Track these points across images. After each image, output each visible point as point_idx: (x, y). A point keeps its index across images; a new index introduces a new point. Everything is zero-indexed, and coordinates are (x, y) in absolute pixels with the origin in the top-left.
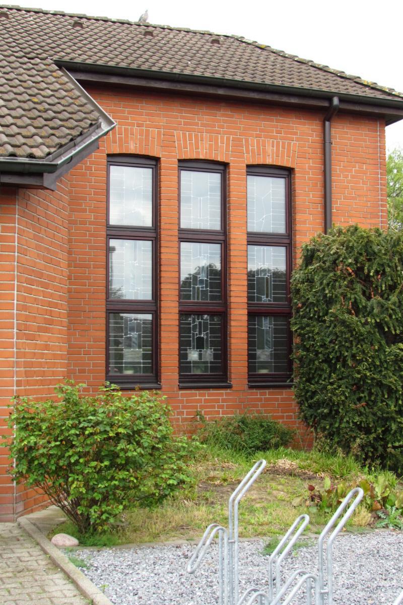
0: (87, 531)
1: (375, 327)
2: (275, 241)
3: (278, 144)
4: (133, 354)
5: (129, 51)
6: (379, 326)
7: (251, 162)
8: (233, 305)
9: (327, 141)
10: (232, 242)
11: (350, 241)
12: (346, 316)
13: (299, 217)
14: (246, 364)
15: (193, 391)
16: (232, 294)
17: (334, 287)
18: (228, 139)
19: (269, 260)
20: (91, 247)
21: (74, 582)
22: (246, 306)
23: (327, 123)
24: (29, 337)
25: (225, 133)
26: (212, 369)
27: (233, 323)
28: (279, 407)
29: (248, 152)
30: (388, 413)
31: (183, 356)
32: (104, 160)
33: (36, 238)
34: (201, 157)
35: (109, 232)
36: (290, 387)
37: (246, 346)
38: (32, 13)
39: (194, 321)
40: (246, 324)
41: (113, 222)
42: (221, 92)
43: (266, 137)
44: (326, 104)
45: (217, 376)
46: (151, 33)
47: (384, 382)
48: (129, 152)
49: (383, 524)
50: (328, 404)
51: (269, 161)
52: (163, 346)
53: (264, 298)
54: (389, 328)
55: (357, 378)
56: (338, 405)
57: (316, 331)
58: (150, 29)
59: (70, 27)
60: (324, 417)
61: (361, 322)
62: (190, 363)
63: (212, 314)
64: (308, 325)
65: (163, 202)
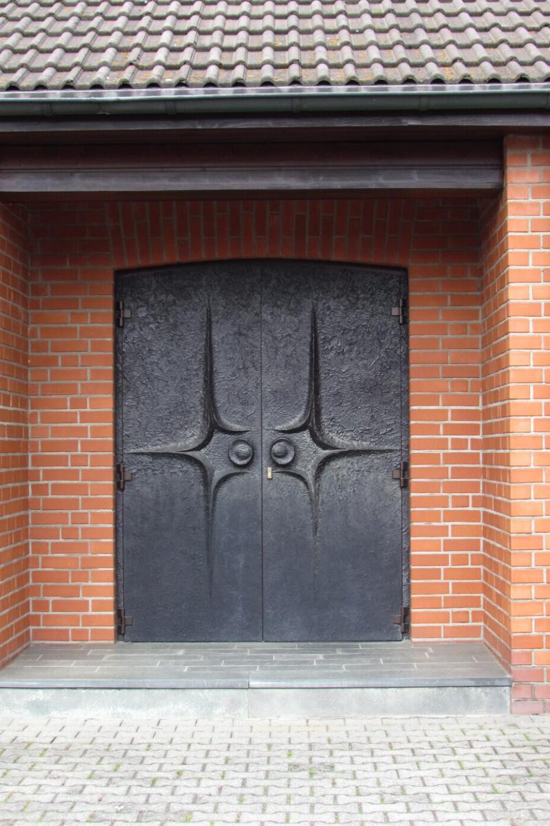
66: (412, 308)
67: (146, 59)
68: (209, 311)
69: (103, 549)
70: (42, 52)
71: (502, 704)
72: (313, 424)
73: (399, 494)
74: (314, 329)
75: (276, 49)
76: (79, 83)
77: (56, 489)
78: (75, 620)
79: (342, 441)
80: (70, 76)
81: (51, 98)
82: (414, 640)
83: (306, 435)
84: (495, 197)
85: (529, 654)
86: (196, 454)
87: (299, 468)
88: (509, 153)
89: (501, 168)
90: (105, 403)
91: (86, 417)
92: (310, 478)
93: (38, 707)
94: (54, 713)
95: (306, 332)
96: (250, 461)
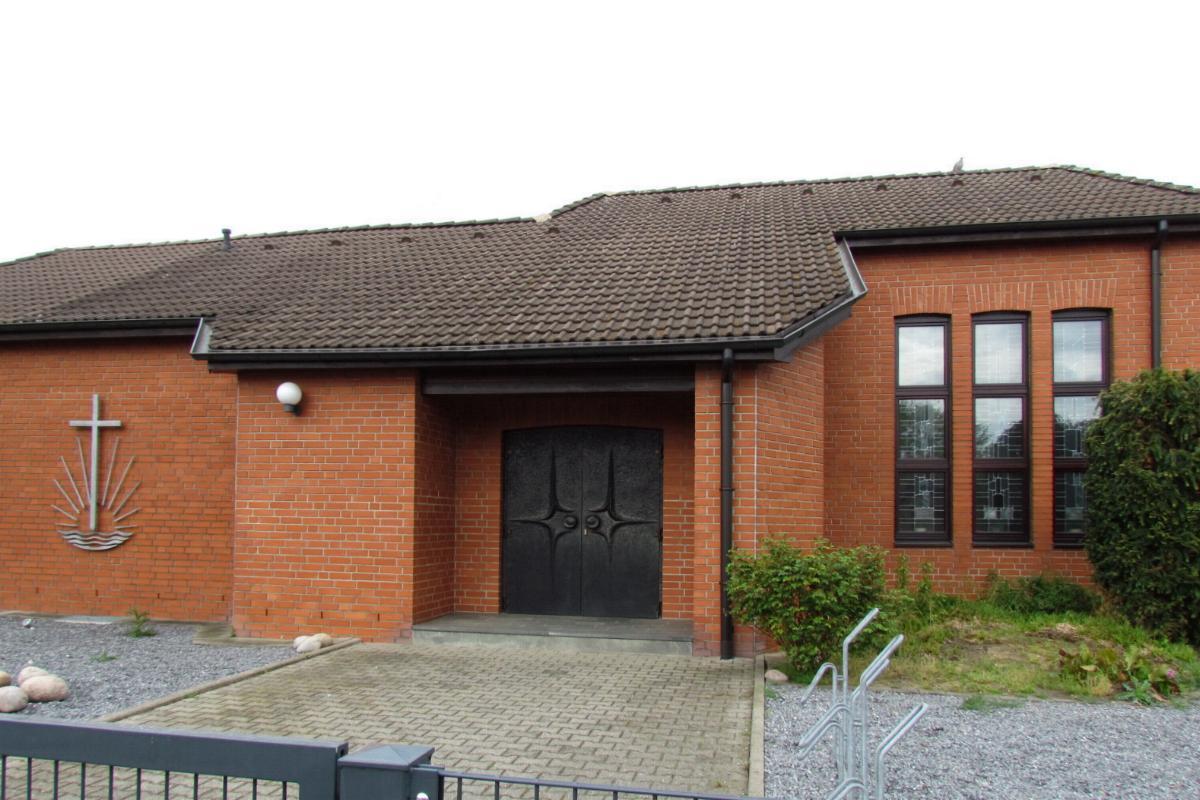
0: (798, 674)
1: (1174, 483)
2: (1087, 390)
3: (1090, 284)
4: (924, 513)
5: (1071, 194)
6: (1179, 481)
7: (1056, 308)
8: (1035, 462)
9: (1155, 272)
10: (1034, 394)
11: (1148, 387)
12: (1140, 471)
13: (1117, 362)
14: (1051, 523)
15: (988, 550)
16: (1035, 449)
17: (1126, 439)
18: (1029, 285)
19: (1079, 412)
20: (878, 410)
21: (179, 699)
22: (1051, 462)
23: (1155, 252)
24: (770, 496)
25: (1025, 279)
26: (1012, 528)
27: (1035, 480)
28: (1076, 569)
29: (1052, 297)
30: (1190, 579)
31: (977, 515)
32: (892, 323)
33: (781, 406)
34: (997, 308)
35: (898, 394)
36: (1081, 547)
37: (1051, 504)
38: (920, 179)
39: (991, 479)
40: (1051, 480)
41: (903, 382)
42: (1017, 236)
43: (1074, 278)
44: (1151, 230)
45: (1019, 534)
46: (1038, 177)
47: (1186, 544)
48: (917, 312)
49: (1126, 697)
50: (1118, 567)
51: (1079, 304)
52: (955, 504)
53: (1075, 452)
54: (1191, 483)
55: (1150, 539)
56: (1129, 568)
57: (1105, 487)
58: (1037, 174)
59: (1027, 182)
60: (1116, 580)
61: (1156, 477)
62: (986, 521)
63: (938, 472)
64: (1097, 481)
65: (954, 359)
66: (665, 450)
67: (677, 324)
68: (553, 452)
69: (494, 567)
70: (618, 321)
71: (688, 651)
72: (610, 507)
73: (658, 544)
74: (611, 460)
75: (752, 316)
76: (609, 338)
77: (469, 537)
78: (477, 601)
79: (626, 517)
80: (573, 335)
81: (578, 346)
82: (664, 618)
83: (606, 514)
84: (690, 398)
85: (704, 626)
86: (547, 522)
87: (602, 529)
88: (696, 374)
89: (693, 380)
90: (497, 496)
91: (486, 503)
92: (608, 535)
93: (438, 640)
94: (446, 644)
95: (607, 460)
96: (576, 525)
